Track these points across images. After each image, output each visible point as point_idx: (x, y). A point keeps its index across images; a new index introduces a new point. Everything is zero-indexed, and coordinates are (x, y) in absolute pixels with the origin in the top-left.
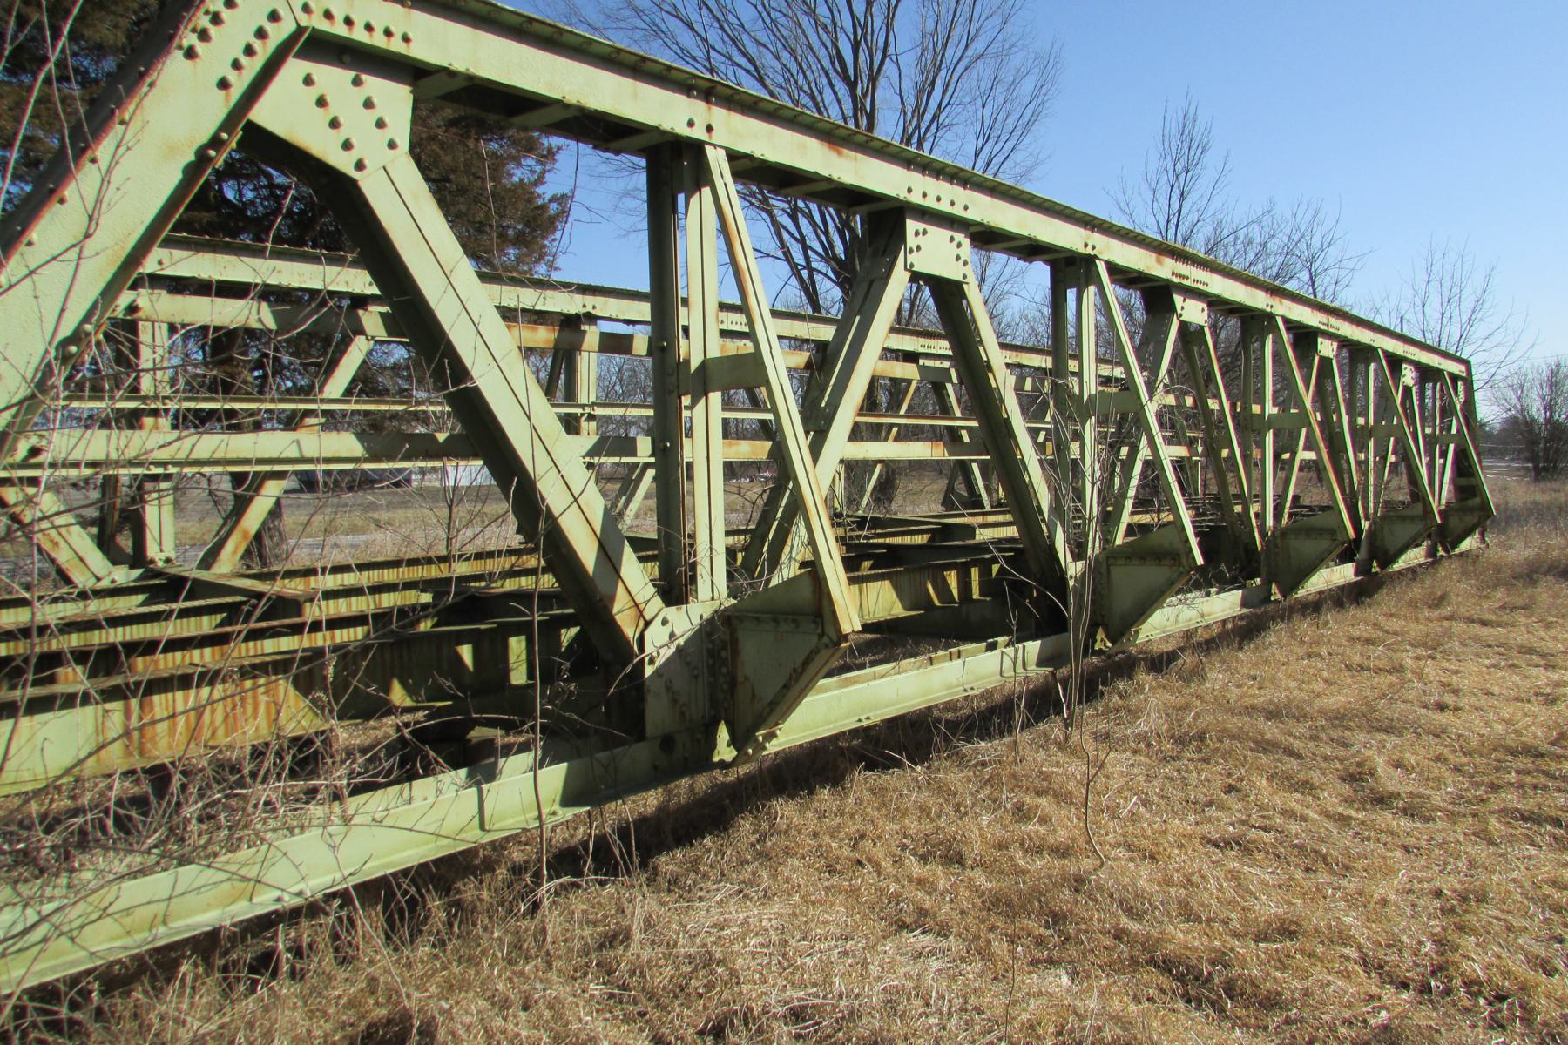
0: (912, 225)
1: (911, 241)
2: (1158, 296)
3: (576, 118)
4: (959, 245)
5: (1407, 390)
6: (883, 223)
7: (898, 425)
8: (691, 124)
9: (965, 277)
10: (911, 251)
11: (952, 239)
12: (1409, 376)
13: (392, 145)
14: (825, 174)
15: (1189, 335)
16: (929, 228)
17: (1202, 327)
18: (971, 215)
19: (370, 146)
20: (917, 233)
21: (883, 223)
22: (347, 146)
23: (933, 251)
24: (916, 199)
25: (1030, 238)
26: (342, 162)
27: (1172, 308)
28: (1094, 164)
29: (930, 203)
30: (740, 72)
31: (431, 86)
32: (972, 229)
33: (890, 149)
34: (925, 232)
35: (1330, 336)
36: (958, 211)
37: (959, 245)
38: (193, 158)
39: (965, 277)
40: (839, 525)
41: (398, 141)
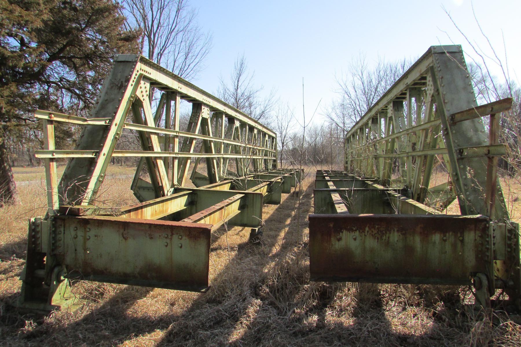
0: (203, 107)
1: (203, 110)
22: (143, 96)
26: (142, 99)
27: (234, 123)
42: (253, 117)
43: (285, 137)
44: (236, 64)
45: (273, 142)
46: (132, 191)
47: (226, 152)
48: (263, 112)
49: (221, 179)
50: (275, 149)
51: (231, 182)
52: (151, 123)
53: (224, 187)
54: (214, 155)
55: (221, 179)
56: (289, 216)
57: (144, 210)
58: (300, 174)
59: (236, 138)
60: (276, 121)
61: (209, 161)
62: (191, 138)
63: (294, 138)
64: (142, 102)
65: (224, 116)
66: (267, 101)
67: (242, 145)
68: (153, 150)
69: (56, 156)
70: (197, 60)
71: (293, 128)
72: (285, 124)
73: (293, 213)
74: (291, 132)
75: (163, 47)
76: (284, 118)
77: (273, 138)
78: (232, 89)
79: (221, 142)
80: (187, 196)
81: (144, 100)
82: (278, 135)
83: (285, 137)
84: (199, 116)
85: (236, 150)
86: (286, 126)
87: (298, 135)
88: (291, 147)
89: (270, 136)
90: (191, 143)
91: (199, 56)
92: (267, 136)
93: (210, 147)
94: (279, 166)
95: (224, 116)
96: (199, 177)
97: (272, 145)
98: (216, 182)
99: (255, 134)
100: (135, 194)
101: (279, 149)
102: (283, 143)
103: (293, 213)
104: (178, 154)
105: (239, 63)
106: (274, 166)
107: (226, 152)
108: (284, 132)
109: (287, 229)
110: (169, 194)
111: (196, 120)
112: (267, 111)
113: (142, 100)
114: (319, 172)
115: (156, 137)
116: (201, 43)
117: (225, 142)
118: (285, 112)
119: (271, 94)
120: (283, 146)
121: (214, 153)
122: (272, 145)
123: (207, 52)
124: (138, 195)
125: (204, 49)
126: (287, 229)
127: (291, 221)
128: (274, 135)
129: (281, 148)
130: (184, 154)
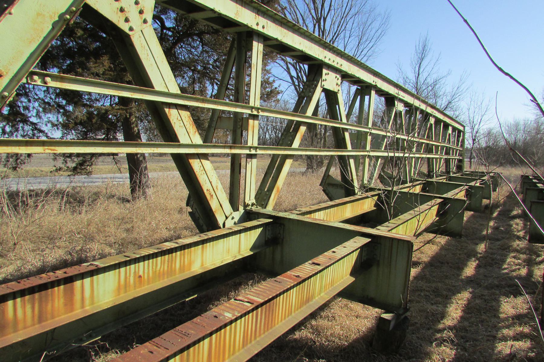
0: (325, 71)
1: (324, 77)
2: (390, 100)
3: (279, 45)
4: (338, 79)
5: (449, 135)
6: (316, 68)
7: (415, 157)
8: (257, 24)
9: (338, 91)
10: (324, 80)
11: (336, 77)
12: (432, 120)
13: (145, 22)
14: (275, 37)
15: (398, 115)
16: (330, 73)
17: (401, 112)
18: (405, 99)
19: (136, 21)
20: (326, 74)
21: (316, 68)
22: (127, 20)
23: (330, 81)
24: (327, 61)
25: (358, 78)
26: (125, 27)
27: (394, 105)
28: (392, 62)
29: (330, 63)
30: (343, 42)
31: (269, 43)
32: (269, 43)
33: (301, 30)
34: (328, 74)
35: (401, 101)
36: (338, 66)
37: (338, 79)
38: (57, 19)
39: (338, 91)
40: (7, 157)
41: (148, 20)
42: (438, 107)
43: (477, 132)
44: (418, 48)
45: (459, 136)
46: (321, 187)
47: (418, 151)
48: (450, 103)
49: (363, 187)
50: (462, 146)
51: (378, 195)
52: (344, 120)
53: (363, 203)
54: (349, 151)
55: (363, 187)
56: (472, 254)
57: (78, 284)
58: (496, 181)
59: (398, 129)
60: (467, 113)
61: (343, 161)
62: (297, 121)
63: (489, 134)
64: (128, 36)
65: (373, 93)
66: (455, 89)
67: (388, 134)
68: (347, 148)
69: (259, 152)
70: (371, 45)
71: (488, 122)
72: (477, 119)
73: (481, 247)
74: (483, 128)
75: (335, 34)
76: (477, 110)
77: (459, 131)
78: (412, 77)
79: (366, 133)
80: (260, 230)
81: (131, 29)
82: (468, 129)
83: (477, 132)
84: (316, 86)
85: (429, 149)
86: (479, 121)
87: (494, 131)
88: (484, 145)
89: (454, 129)
90: (296, 130)
91: (373, 40)
92: (450, 129)
93: (344, 139)
94: (467, 168)
95: (373, 93)
96: (333, 182)
97: (458, 141)
98: (354, 194)
99: (431, 125)
100: (324, 191)
101: (468, 144)
102: (474, 140)
103: (481, 247)
104: (256, 148)
105: (420, 45)
106: (460, 168)
107: (418, 151)
108: (476, 127)
109: (464, 296)
110: (230, 223)
111: (310, 92)
112: (456, 100)
113: (127, 31)
114: (525, 179)
115: (186, 114)
116: (376, 25)
117: (374, 131)
118: (479, 104)
119: (461, 80)
120: (473, 144)
121: (349, 147)
122: (458, 141)
123: (383, 33)
124: (327, 191)
125: (380, 31)
126: (464, 296)
127: (478, 267)
128: (461, 128)
129: (472, 145)
130: (281, 149)
